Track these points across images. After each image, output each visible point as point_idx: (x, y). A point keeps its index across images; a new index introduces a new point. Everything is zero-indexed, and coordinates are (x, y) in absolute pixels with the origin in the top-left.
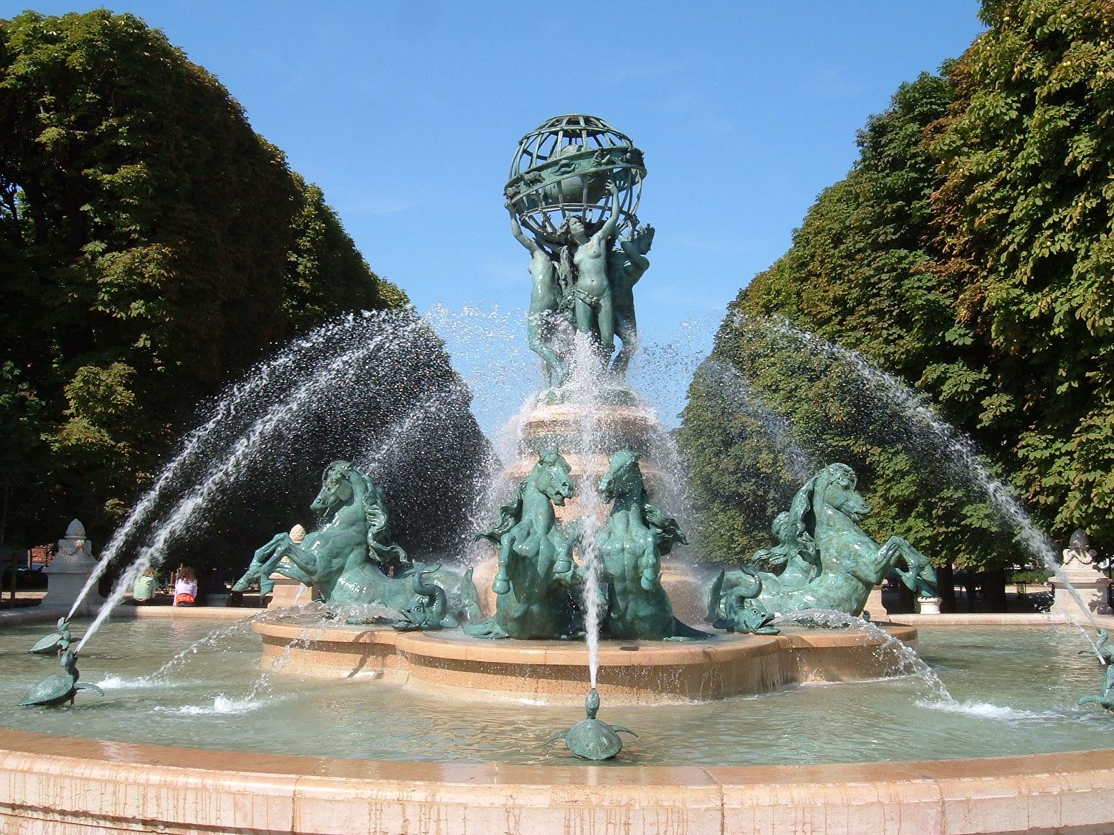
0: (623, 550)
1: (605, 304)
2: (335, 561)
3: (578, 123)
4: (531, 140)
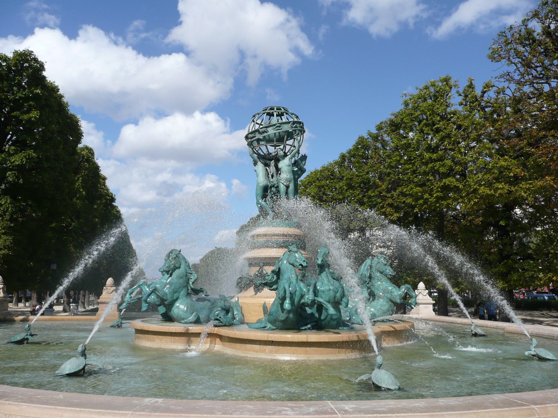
0: (330, 289)
1: (292, 186)
2: (175, 295)
3: (274, 109)
4: (260, 115)
